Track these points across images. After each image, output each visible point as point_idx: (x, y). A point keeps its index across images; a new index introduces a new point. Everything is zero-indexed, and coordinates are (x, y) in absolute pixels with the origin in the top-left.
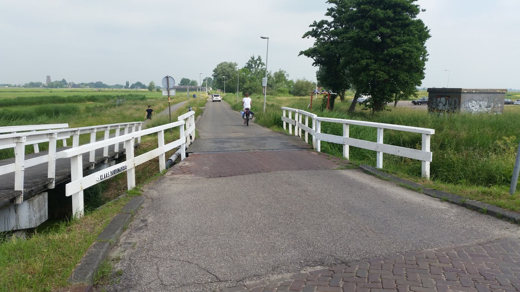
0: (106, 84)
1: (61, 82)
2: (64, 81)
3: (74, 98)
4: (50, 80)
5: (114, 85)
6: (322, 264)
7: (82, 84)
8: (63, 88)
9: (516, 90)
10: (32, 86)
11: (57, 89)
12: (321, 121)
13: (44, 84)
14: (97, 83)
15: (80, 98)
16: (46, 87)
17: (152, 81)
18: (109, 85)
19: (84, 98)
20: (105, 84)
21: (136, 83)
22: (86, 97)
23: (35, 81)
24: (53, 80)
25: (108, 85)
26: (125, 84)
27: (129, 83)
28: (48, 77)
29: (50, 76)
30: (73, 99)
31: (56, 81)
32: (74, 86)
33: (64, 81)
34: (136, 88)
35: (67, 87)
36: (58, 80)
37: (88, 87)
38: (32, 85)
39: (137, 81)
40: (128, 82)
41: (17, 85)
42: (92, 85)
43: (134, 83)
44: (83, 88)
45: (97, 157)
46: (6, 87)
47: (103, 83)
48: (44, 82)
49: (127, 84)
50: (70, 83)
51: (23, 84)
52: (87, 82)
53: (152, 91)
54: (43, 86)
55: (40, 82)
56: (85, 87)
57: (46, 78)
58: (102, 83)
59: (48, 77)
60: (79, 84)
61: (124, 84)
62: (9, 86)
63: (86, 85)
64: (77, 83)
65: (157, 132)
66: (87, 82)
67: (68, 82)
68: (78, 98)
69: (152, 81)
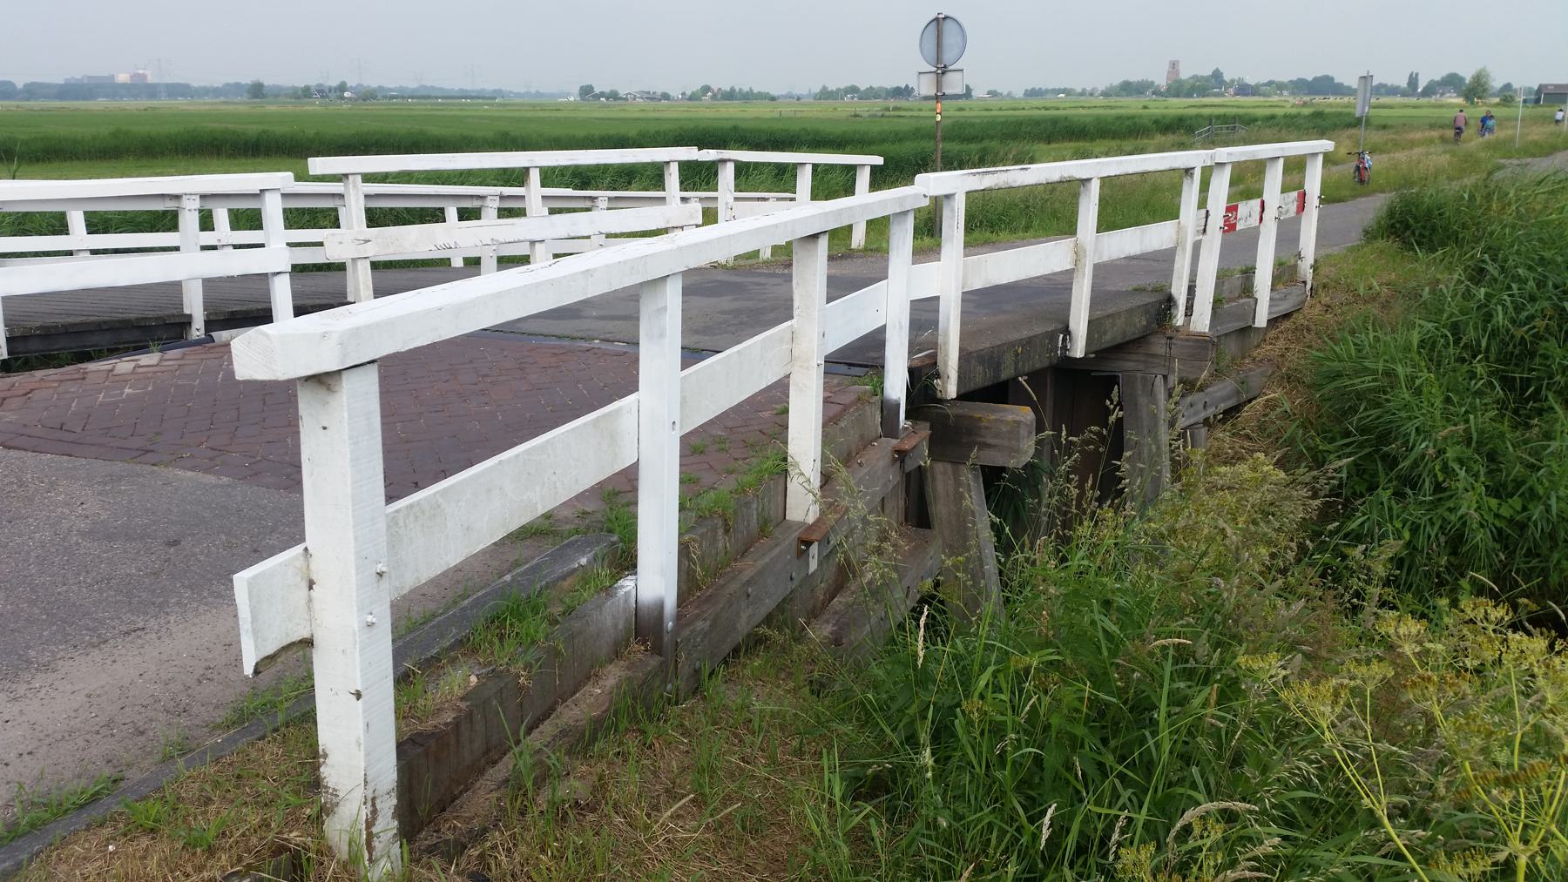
0: (1346, 84)
1: (1207, 79)
2: (1217, 75)
3: (1118, 123)
4: (1177, 73)
5: (20, 85)
6: (577, 532)
7: (1270, 83)
8: (1207, 96)
9: (407, 88)
10: (1125, 93)
11: (1191, 100)
12: (541, 168)
13: (1158, 86)
14: (1316, 79)
15: (1135, 124)
16: (1161, 94)
17: (1484, 69)
18: (195, 84)
19: (1150, 124)
20: (1342, 84)
21: (1442, 78)
22: (1156, 122)
23: (1135, 77)
24: (1185, 74)
25: (1341, 85)
26: (1403, 83)
27: (1419, 77)
28: (1174, 65)
29: (1178, 62)
30: (1113, 128)
31: (1195, 77)
32: (1244, 89)
33: (1217, 75)
34: (1442, 94)
35: (1222, 95)
36: (1200, 73)
37: (1285, 93)
38: (1127, 88)
39: (1448, 72)
40: (1417, 74)
41: (1089, 89)
42: (1299, 86)
43: (1438, 78)
44: (1269, 96)
45: (1275, 309)
46: (1061, 98)
47: (1337, 80)
48: (1161, 81)
49: (1413, 81)
50: (1233, 81)
51: (1101, 87)
52: (1285, 78)
53: (1472, 103)
54: (1153, 93)
55: (1150, 80)
56: (1276, 94)
57: (1166, 67)
58: (1332, 79)
59: (1174, 65)
60: (1258, 86)
61: (1403, 83)
62: (1067, 92)
63: (1281, 87)
64: (1251, 80)
65: (888, 217)
66: (1285, 77)
67: (1227, 78)
68: (1129, 122)
69: (1484, 69)
